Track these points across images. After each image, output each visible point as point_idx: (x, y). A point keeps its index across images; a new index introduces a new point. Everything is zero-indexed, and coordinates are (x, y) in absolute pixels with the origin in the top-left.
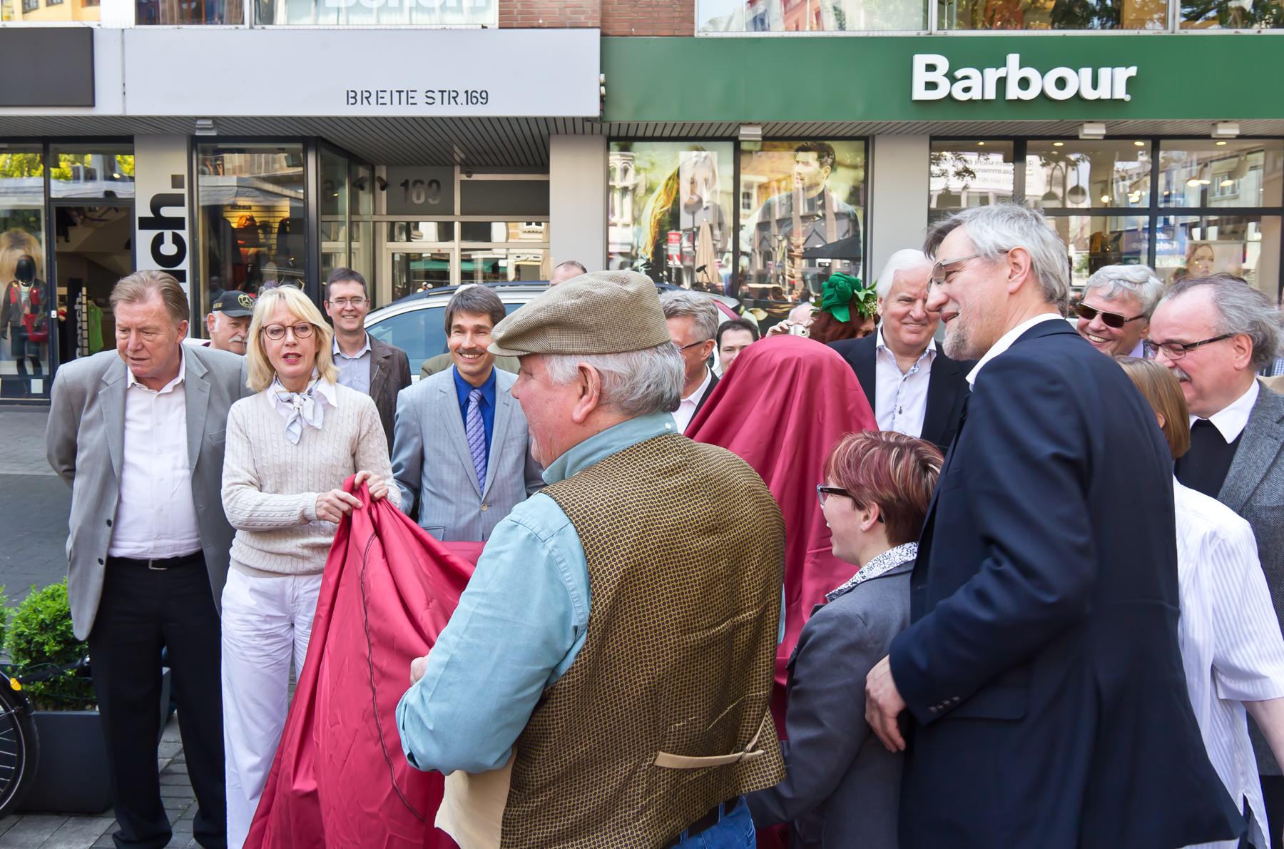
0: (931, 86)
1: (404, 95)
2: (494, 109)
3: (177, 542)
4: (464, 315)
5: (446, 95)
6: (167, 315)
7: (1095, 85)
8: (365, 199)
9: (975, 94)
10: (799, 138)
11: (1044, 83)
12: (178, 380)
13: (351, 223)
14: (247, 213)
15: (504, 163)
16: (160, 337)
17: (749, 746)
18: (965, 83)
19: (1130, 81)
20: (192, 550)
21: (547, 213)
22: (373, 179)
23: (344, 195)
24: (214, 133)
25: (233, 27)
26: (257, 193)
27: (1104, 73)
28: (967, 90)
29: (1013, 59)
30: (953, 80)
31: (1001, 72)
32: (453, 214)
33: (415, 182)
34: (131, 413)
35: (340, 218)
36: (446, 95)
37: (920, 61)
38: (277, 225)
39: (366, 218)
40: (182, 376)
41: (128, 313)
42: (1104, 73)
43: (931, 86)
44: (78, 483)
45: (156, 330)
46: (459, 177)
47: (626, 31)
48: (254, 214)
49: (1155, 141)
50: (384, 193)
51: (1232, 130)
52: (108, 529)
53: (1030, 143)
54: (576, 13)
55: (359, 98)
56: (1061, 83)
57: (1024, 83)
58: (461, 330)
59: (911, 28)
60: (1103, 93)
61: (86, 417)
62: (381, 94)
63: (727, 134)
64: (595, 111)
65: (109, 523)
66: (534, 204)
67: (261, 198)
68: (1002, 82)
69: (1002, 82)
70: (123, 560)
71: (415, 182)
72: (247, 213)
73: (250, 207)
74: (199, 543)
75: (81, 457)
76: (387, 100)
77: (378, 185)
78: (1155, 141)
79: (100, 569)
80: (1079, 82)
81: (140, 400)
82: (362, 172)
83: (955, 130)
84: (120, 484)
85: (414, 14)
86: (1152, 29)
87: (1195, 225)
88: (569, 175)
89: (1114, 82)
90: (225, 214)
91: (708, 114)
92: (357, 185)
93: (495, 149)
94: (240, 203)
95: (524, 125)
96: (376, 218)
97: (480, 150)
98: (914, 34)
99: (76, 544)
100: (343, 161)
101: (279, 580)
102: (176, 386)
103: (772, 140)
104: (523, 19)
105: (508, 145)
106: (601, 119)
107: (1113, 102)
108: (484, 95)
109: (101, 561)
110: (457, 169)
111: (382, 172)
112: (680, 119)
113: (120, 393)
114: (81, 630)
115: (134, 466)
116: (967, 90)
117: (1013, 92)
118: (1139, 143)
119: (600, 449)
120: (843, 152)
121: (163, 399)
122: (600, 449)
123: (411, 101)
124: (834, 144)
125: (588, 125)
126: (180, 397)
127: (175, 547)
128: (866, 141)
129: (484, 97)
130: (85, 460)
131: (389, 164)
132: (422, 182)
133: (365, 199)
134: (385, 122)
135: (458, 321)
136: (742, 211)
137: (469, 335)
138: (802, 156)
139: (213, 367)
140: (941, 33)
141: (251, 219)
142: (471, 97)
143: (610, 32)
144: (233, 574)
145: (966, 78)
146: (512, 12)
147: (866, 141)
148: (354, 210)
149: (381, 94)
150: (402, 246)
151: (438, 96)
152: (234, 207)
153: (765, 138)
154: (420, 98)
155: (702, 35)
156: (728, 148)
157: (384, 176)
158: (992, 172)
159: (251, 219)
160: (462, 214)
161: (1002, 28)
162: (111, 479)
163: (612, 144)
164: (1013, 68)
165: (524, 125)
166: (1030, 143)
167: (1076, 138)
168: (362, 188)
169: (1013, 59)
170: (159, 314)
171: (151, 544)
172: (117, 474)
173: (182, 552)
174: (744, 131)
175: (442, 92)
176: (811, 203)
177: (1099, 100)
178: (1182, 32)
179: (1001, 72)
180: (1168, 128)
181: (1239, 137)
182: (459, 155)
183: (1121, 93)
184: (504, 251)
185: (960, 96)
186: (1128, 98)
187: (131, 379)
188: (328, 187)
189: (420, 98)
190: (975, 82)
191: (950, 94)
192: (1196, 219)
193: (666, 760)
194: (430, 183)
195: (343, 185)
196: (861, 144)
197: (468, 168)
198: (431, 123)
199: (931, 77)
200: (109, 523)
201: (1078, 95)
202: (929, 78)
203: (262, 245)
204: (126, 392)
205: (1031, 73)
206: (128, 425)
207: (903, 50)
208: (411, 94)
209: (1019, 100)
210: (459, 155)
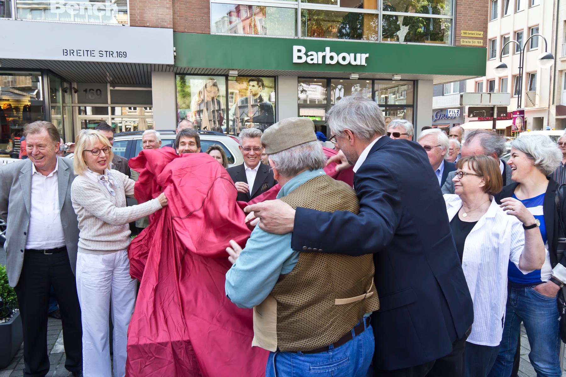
0: (300, 58)
1: (89, 52)
2: (130, 59)
3: (56, 241)
4: (185, 137)
5: (108, 53)
6: (50, 140)
7: (355, 60)
8: (68, 97)
9: (315, 61)
11: (338, 58)
13: (63, 106)
15: (133, 83)
16: (47, 148)
17: (368, 291)
18: (311, 57)
19: (367, 59)
21: (151, 103)
22: (71, 88)
23: (60, 94)
25: (7, 19)
27: (358, 55)
28: (312, 60)
29: (328, 49)
30: (307, 56)
31: (324, 54)
32: (107, 103)
33: (90, 90)
34: (34, 186)
35: (58, 105)
36: (108, 53)
37: (295, 48)
38: (22, 108)
39: (68, 105)
41: (32, 139)
42: (358, 55)
43: (300, 58)
44: (10, 218)
45: (44, 146)
46: (110, 88)
48: (11, 103)
49: (373, 80)
50: (76, 94)
52: (25, 236)
53: (332, 80)
54: (163, 22)
55: (69, 53)
56: (344, 58)
57: (332, 58)
58: (184, 144)
59: (290, 35)
60: (358, 63)
61: (13, 188)
62: (79, 52)
63: (223, 73)
64: (172, 62)
66: (146, 100)
67: (13, 96)
68: (324, 57)
69: (324, 57)
70: (32, 250)
71: (90, 90)
73: (9, 100)
74: (64, 242)
75: (10, 205)
77: (73, 91)
78: (373, 80)
80: (350, 58)
81: (38, 180)
82: (66, 85)
83: (307, 74)
84: (30, 216)
86: (372, 40)
89: (361, 59)
92: (64, 91)
93: (123, 77)
94: (3, 98)
96: (73, 105)
98: (293, 38)
99: (9, 245)
100: (57, 80)
101: (114, 254)
102: (54, 173)
103: (241, 77)
105: (126, 75)
106: (174, 66)
108: (125, 54)
109: (22, 251)
110: (109, 85)
111: (75, 85)
112: (205, 67)
113: (29, 177)
114: (13, 284)
115: (36, 208)
117: (328, 61)
118: (368, 81)
119: (295, 183)
122: (295, 183)
123: (92, 55)
124: (263, 79)
125: (168, 68)
126: (55, 178)
129: (125, 55)
130: (13, 207)
131: (78, 82)
132: (93, 90)
135: (182, 140)
137: (187, 145)
138: (252, 83)
140: (302, 38)
141: (10, 105)
142: (119, 54)
143: (177, 30)
144: (79, 254)
145: (312, 55)
148: (64, 102)
149: (79, 52)
150: (83, 116)
151: (104, 53)
153: (239, 76)
154: (96, 54)
155: (213, 34)
156: (224, 78)
157: (76, 87)
159: (10, 105)
160: (112, 103)
162: (26, 214)
163: (177, 76)
166: (332, 80)
167: (349, 79)
168: (66, 92)
169: (328, 49)
170: (46, 139)
171: (44, 243)
173: (59, 246)
175: (106, 52)
176: (256, 101)
177: (356, 65)
178: (383, 42)
179: (324, 54)
180: (378, 76)
181: (401, 80)
182: (109, 79)
183: (364, 63)
185: (310, 62)
186: (366, 65)
187: (34, 170)
188: (53, 91)
189: (96, 54)
190: (315, 57)
192: (384, 108)
193: (339, 302)
194: (97, 90)
195: (58, 91)
197: (113, 84)
199: (300, 54)
200: (25, 234)
201: (350, 63)
202: (299, 54)
205: (334, 54)
206: (33, 191)
207: (288, 44)
208: (92, 52)
209: (330, 64)
210: (109, 79)
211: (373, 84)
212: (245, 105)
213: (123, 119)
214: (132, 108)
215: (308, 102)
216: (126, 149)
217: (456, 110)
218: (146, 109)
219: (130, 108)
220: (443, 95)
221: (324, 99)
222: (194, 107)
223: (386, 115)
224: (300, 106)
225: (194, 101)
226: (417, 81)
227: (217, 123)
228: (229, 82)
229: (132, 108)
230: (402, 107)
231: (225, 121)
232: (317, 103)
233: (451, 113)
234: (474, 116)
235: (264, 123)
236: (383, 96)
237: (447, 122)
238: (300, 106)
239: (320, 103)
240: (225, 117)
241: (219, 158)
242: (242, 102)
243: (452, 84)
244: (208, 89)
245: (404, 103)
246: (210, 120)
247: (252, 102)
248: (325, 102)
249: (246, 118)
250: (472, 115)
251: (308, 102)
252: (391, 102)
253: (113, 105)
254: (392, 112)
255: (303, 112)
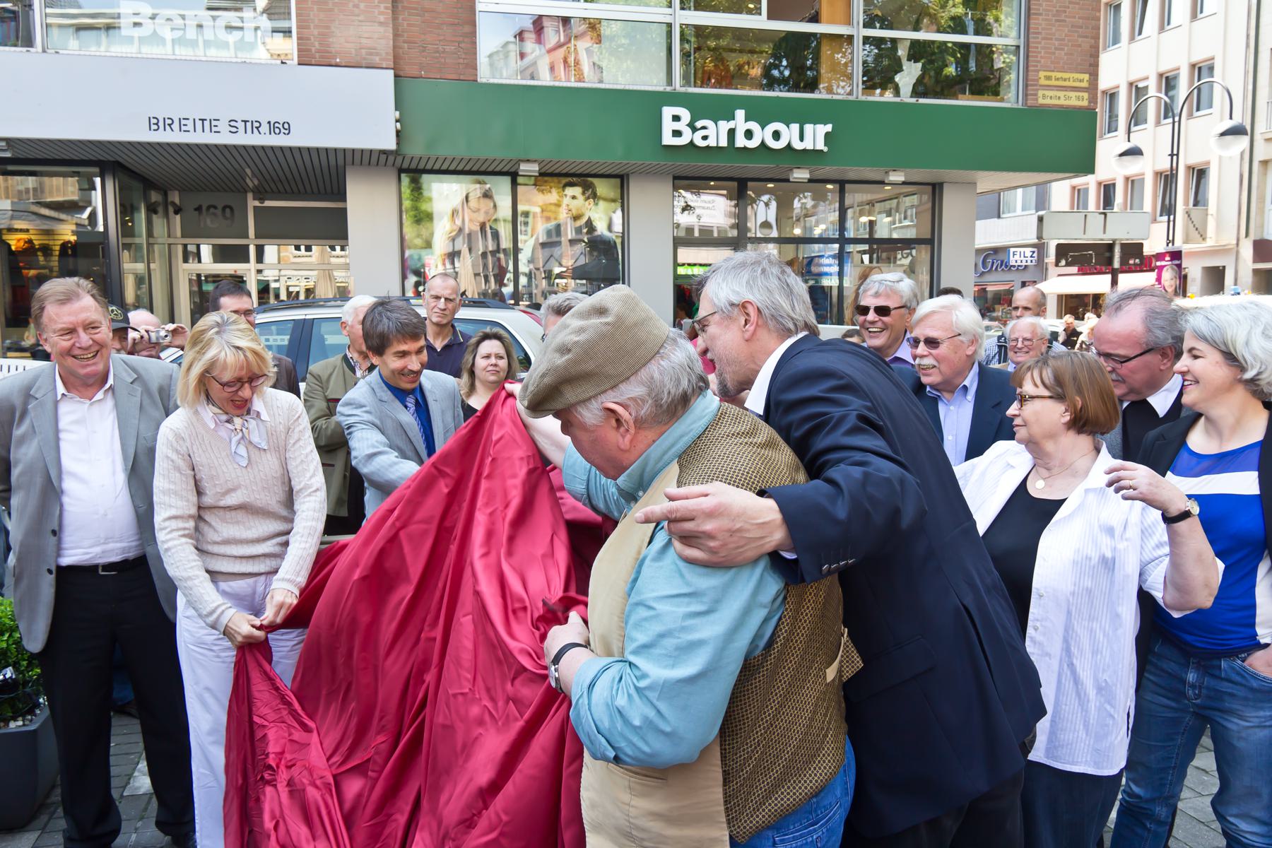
0: (677, 133)
1: (207, 124)
5: (249, 125)
7: (802, 139)
9: (711, 142)
10: (567, 175)
11: (763, 134)
12: (107, 386)
14: (24, 236)
15: (305, 190)
18: (703, 133)
19: (827, 134)
20: (131, 555)
21: (346, 237)
22: (166, 204)
23: (142, 216)
24: (8, 155)
25: (24, 49)
26: (34, 217)
28: (705, 138)
29: (740, 114)
30: (694, 130)
31: (731, 124)
32: (247, 237)
34: (63, 424)
35: (137, 240)
36: (249, 125)
37: (668, 112)
38: (58, 248)
39: (160, 240)
40: (110, 381)
42: (809, 128)
43: (677, 133)
46: (252, 203)
47: (416, 73)
48: (33, 237)
49: (842, 184)
50: (178, 217)
51: (897, 177)
52: (53, 539)
53: (750, 184)
54: (371, 54)
55: (161, 124)
56: (776, 135)
57: (749, 134)
59: (653, 81)
60: (808, 144)
62: (183, 122)
63: (505, 169)
64: (391, 144)
65: (54, 533)
66: (333, 229)
67: (38, 222)
68: (732, 133)
69: (732, 133)
71: (209, 208)
72: (24, 236)
73: (27, 231)
76: (190, 127)
77: (171, 210)
78: (842, 184)
79: (51, 579)
80: (790, 134)
82: (155, 197)
83: (692, 171)
85: (177, 47)
87: (864, 252)
88: (369, 206)
89: (815, 136)
90: (4, 237)
91: (492, 151)
92: (152, 210)
94: (16, 226)
95: (323, 157)
96: (171, 241)
97: (275, 178)
99: (19, 559)
100: (136, 185)
104: (321, 57)
106: (396, 153)
107: (816, 153)
109: (50, 571)
110: (250, 196)
111: (175, 197)
113: (50, 406)
115: (74, 475)
116: (705, 138)
117: (741, 141)
118: (830, 186)
119: (682, 436)
120: (602, 187)
121: (96, 408)
122: (682, 436)
123: (214, 129)
124: (596, 181)
125: (383, 157)
126: (110, 403)
127: (124, 550)
128: (622, 179)
130: (20, 475)
131: (183, 190)
132: (215, 207)
133: (158, 222)
134: (186, 149)
136: (520, 237)
138: (570, 191)
139: (142, 372)
141: (30, 241)
142: (273, 127)
143: (401, 73)
145: (704, 128)
146: (310, 50)
147: (622, 179)
148: (150, 234)
149: (183, 122)
150: (192, 266)
151: (241, 125)
152: (11, 230)
153: (542, 174)
154: (223, 126)
155: (484, 81)
157: (177, 201)
158: (713, 209)
159: (30, 241)
161: (714, 87)
162: (51, 492)
163: (403, 176)
164: (740, 121)
165: (323, 157)
166: (750, 184)
167: (787, 180)
168: (156, 212)
169: (740, 114)
171: (97, 550)
172: (56, 484)
174: (524, 167)
175: (245, 122)
176: (579, 230)
177: (805, 150)
179: (731, 124)
180: (852, 175)
181: (904, 183)
183: (821, 145)
184: (276, 272)
185: (700, 143)
186: (826, 149)
187: (61, 389)
188: (126, 209)
189: (223, 126)
191: (692, 142)
192: (866, 247)
194: (224, 208)
195: (138, 209)
196: (618, 181)
197: (261, 194)
198: (214, 150)
199: (677, 126)
200: (54, 533)
201: (789, 146)
202: (675, 126)
203: (44, 268)
204: (56, 403)
206: (62, 435)
207: (651, 103)
208: (214, 123)
209: (745, 148)
211: (842, 192)
212: (555, 239)
213: (283, 273)
214: (303, 248)
215: (697, 234)
216: (290, 341)
217: (1028, 251)
218: (333, 248)
219: (297, 248)
220: (999, 217)
221: (732, 227)
222: (441, 244)
223: (871, 261)
224: (678, 242)
225: (442, 230)
226: (941, 185)
227: (492, 280)
228: (520, 189)
229: (303, 248)
230: (907, 244)
231: (510, 276)
232: (716, 235)
233: (1017, 257)
234: (1068, 264)
235: (597, 280)
236: (864, 219)
237: (1008, 276)
238: (678, 242)
239: (723, 235)
240: (511, 268)
241: (502, 358)
242: (549, 233)
243: (1020, 191)
244: (473, 203)
245: (911, 234)
246: (476, 275)
247: (570, 234)
248: (735, 233)
249: (557, 270)
250: (1063, 262)
251: (697, 234)
252: (882, 232)
253: (260, 242)
254: (884, 255)
255: (685, 254)
